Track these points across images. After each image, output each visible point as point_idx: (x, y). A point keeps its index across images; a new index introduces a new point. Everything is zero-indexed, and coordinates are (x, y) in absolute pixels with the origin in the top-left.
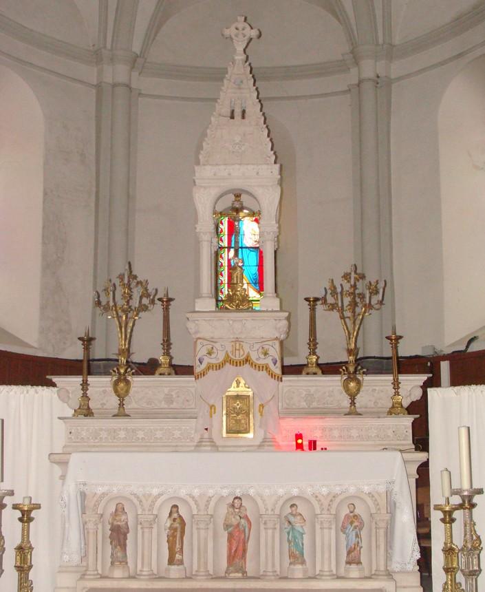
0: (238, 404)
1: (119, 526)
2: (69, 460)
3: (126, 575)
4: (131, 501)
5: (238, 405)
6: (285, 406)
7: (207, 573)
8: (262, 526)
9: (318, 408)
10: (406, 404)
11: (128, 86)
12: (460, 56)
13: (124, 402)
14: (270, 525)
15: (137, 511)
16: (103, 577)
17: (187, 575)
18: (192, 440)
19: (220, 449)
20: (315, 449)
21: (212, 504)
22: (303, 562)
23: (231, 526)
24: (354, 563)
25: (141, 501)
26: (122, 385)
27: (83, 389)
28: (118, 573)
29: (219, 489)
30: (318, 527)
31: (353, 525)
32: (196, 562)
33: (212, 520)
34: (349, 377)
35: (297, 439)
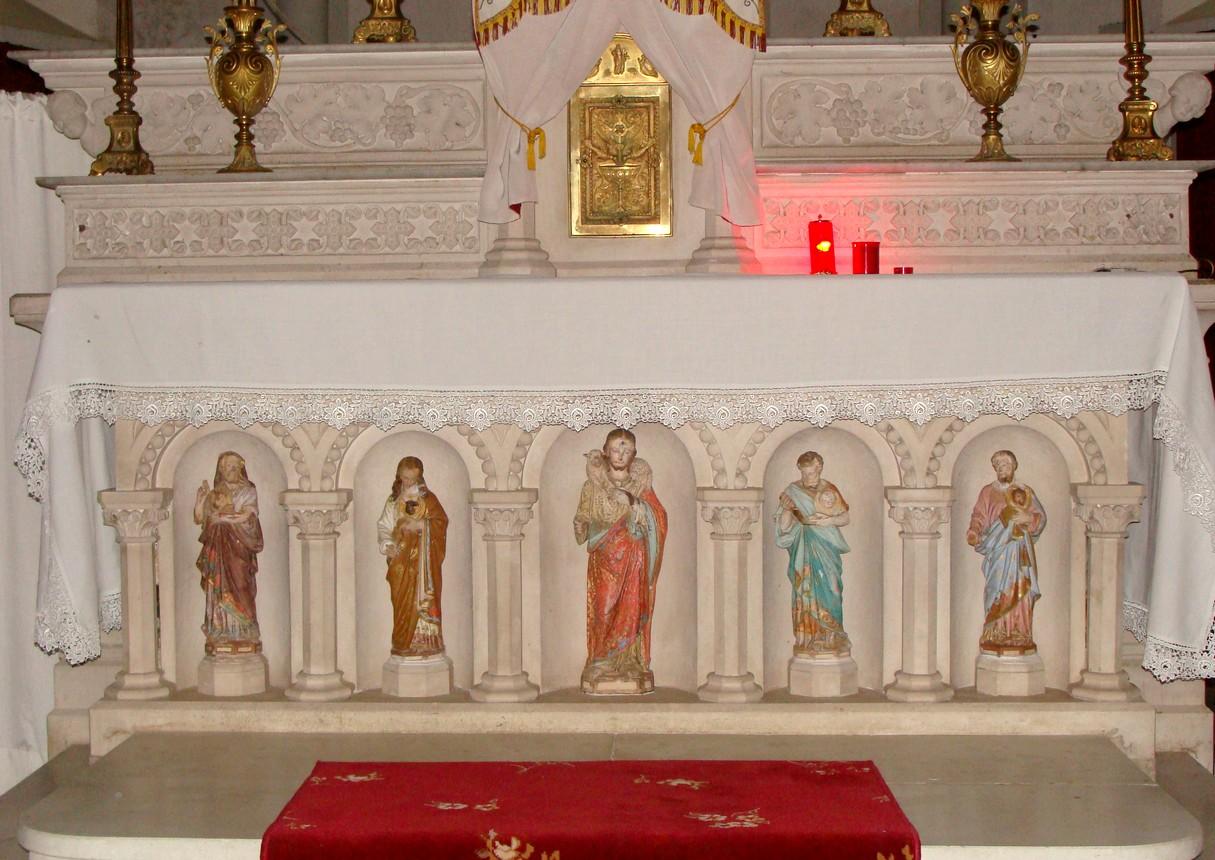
0: (623, 128)
1: (227, 529)
2: (44, 313)
3: (256, 684)
4: (448, 448)
5: (620, 130)
6: (771, 137)
7: (522, 683)
8: (704, 529)
9: (877, 145)
10: (1163, 125)
13: (252, 130)
14: (731, 524)
15: (285, 480)
16: (180, 695)
17: (458, 685)
18: (471, 244)
19: (561, 272)
20: (874, 269)
21: (536, 453)
22: (841, 645)
23: (600, 525)
24: (1011, 647)
25: (295, 447)
26: (243, 73)
27: (117, 89)
28: (229, 679)
29: (560, 405)
31: (1011, 524)
32: (485, 643)
33: (535, 506)
34: (982, 40)
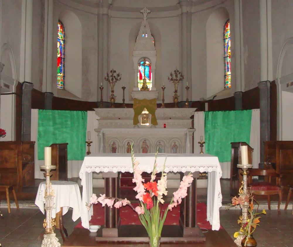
11: (107, 15)
12: (213, 7)
25: (120, 141)
30: (166, 148)
35: (164, 125)
